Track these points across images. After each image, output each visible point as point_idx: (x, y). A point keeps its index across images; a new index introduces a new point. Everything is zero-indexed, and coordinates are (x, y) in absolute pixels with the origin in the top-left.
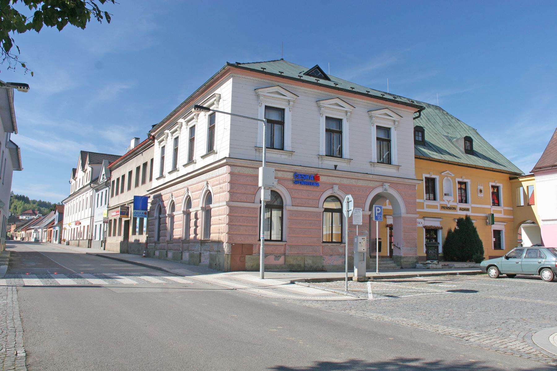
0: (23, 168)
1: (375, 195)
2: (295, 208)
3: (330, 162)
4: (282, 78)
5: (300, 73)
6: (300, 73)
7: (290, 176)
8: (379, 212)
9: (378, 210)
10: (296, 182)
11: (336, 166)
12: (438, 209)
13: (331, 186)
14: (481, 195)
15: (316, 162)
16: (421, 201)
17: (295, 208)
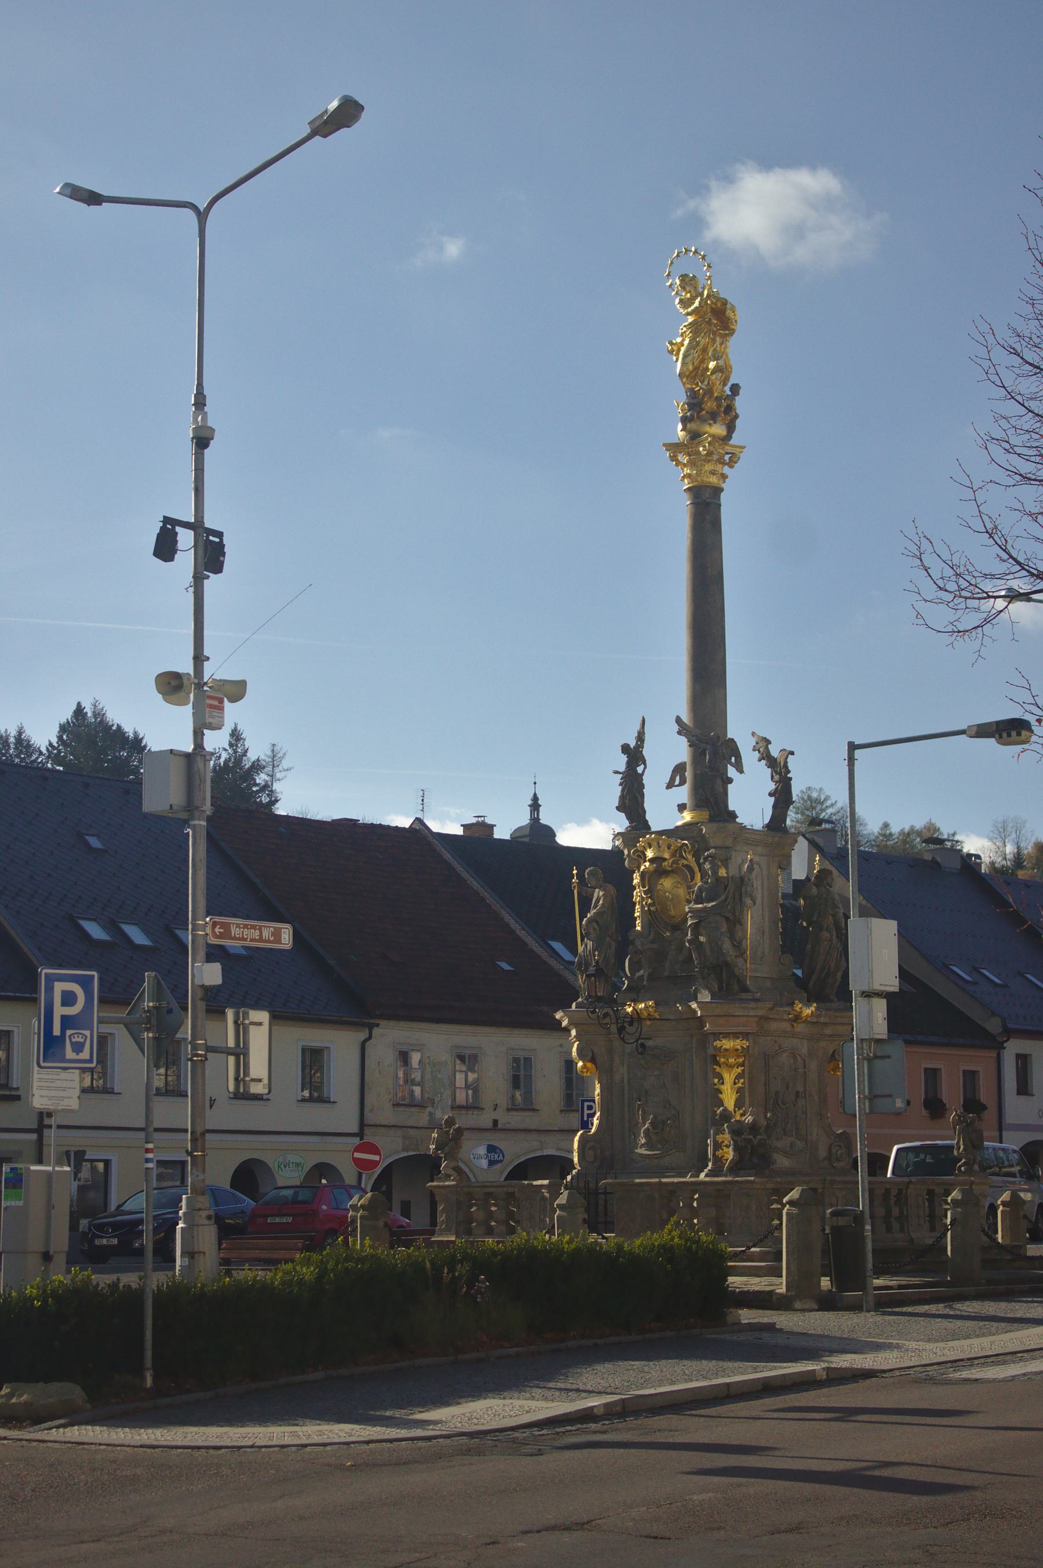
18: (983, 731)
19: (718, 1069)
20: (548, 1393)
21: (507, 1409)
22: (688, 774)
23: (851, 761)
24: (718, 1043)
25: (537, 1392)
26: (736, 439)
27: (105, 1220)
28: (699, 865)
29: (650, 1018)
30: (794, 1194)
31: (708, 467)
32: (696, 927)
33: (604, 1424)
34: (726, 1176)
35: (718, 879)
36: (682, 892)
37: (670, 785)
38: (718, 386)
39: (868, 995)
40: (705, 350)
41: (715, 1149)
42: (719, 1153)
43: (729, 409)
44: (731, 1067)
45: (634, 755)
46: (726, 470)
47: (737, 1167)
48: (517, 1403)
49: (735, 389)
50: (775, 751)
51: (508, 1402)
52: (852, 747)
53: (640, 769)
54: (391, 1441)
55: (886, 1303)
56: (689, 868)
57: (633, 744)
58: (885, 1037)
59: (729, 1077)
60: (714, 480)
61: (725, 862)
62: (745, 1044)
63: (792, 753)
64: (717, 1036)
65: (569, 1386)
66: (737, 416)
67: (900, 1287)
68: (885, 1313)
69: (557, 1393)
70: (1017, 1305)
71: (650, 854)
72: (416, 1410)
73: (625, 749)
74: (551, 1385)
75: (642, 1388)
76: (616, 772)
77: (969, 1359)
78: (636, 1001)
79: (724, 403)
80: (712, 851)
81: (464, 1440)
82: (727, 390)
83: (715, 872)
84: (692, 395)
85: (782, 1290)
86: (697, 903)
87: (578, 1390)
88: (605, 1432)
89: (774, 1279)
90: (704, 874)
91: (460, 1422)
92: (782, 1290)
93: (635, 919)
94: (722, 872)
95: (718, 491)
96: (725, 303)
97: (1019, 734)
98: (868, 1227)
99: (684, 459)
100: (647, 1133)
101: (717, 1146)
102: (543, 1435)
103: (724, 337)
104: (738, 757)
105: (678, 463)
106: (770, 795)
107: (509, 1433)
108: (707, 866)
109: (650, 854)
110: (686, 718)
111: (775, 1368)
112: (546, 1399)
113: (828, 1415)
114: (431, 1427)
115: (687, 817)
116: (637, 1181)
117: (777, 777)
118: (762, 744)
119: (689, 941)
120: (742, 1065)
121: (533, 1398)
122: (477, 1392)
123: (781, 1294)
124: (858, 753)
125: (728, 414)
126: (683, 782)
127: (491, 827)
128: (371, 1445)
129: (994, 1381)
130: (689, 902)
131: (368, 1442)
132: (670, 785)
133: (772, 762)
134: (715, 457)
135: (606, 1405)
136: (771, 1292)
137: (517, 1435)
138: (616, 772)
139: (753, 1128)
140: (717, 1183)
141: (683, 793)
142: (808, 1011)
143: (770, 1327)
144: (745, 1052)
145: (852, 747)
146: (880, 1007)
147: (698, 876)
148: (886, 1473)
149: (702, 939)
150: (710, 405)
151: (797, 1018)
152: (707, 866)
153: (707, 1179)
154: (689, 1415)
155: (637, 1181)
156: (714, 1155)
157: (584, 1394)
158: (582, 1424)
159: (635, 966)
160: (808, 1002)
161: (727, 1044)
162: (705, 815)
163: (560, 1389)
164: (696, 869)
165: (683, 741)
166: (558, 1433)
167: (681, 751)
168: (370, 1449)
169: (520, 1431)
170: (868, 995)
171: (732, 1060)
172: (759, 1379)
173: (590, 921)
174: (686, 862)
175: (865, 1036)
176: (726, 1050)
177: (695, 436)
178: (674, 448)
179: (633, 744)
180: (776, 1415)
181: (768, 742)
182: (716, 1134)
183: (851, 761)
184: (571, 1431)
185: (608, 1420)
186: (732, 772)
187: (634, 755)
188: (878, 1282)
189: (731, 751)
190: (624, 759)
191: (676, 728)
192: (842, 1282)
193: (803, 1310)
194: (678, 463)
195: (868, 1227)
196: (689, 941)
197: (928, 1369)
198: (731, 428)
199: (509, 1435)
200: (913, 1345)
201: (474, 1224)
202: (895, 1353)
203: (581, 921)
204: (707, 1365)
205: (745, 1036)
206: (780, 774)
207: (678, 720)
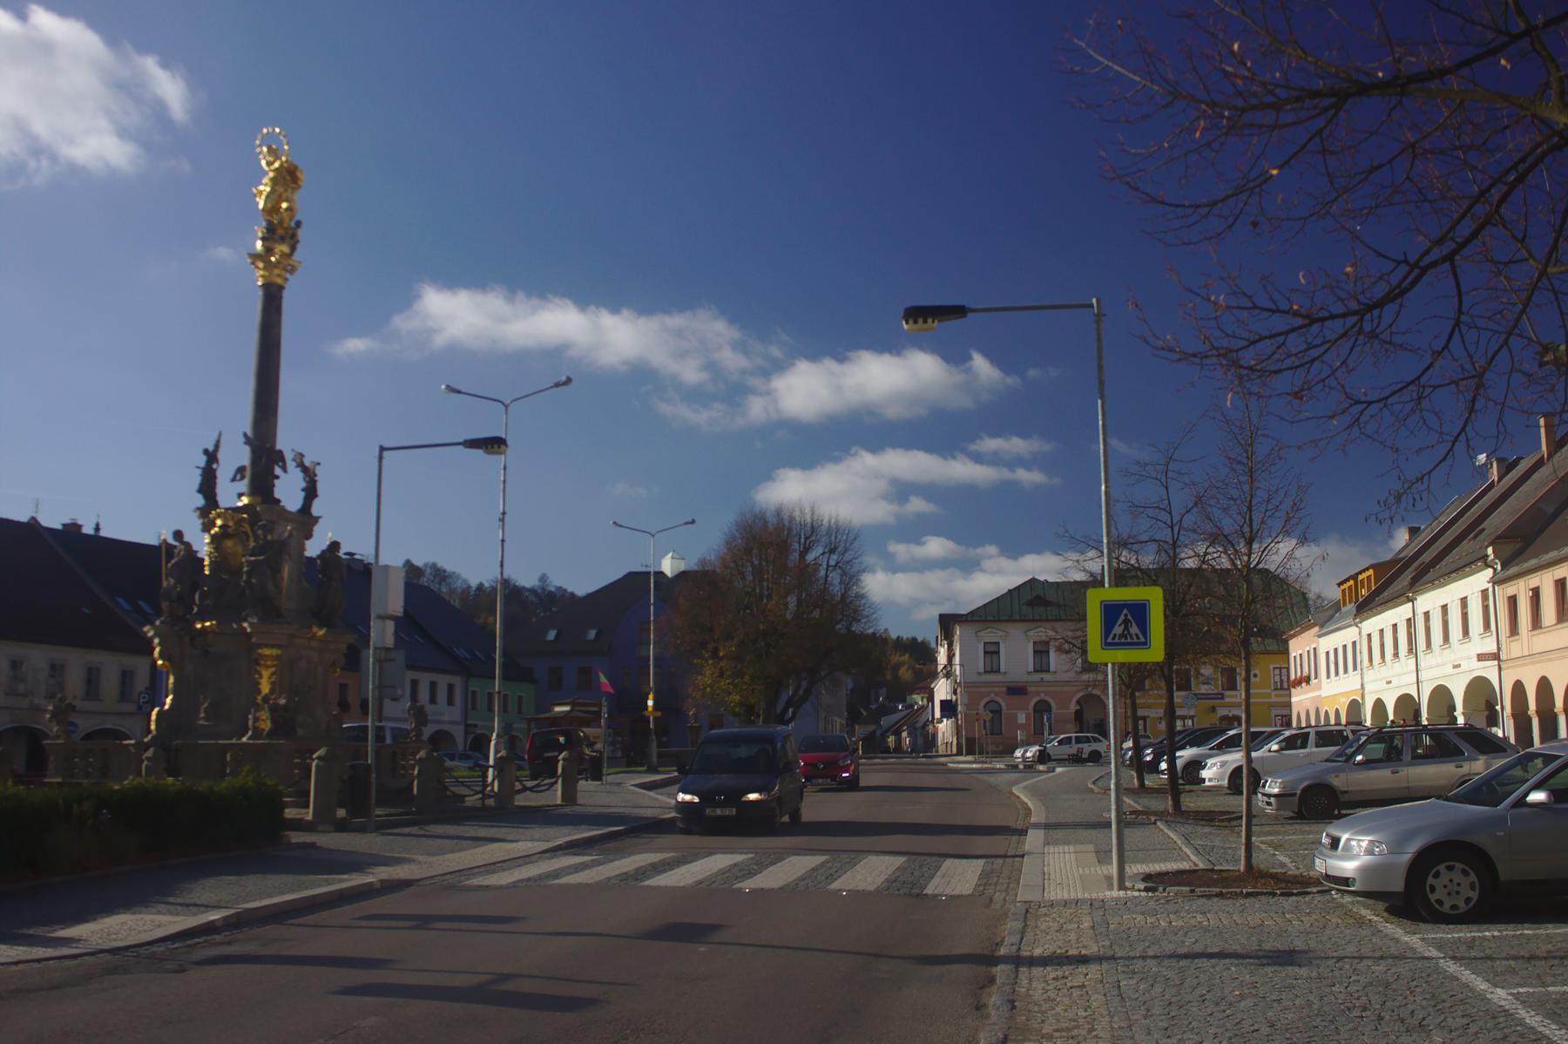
0: (543, 578)
1: (1465, 693)
2: (1059, 711)
3: (1037, 677)
4: (1011, 588)
5: (1400, 479)
6: (1400, 479)
7: (1004, 689)
8: (145, 700)
9: (144, 698)
10: (1008, 694)
11: (1042, 679)
12: (941, 701)
13: (1038, 693)
14: (1258, 679)
15: (1026, 678)
16: (1269, 691)
17: (1059, 711)
18: (473, 444)
19: (258, 668)
20: (172, 908)
21: (139, 923)
22: (248, 473)
23: (381, 458)
24: (260, 651)
25: (162, 907)
26: (297, 256)
27: (961, 766)
28: (252, 530)
29: (213, 632)
30: (321, 752)
31: (276, 271)
32: (249, 573)
33: (226, 935)
34: (264, 739)
35: (266, 542)
36: (240, 549)
37: (234, 480)
38: (287, 220)
39: (382, 617)
40: (280, 195)
41: (254, 722)
42: (257, 724)
43: (294, 236)
44: (267, 667)
45: (212, 456)
46: (288, 276)
47: (272, 734)
48: (149, 917)
49: (298, 224)
50: (307, 463)
51: (139, 916)
52: (382, 449)
53: (214, 466)
54: (39, 961)
55: (382, 827)
56: (246, 533)
57: (211, 448)
58: (392, 646)
59: (266, 674)
60: (279, 281)
61: (271, 531)
62: (279, 652)
63: (319, 464)
64: (260, 646)
65: (188, 901)
66: (298, 241)
67: (387, 815)
68: (383, 834)
69: (179, 908)
70: (467, 828)
71: (219, 522)
72: (56, 927)
73: (206, 452)
74: (171, 900)
75: (247, 902)
76: (198, 467)
77: (468, 869)
78: (204, 621)
79: (290, 232)
80: (264, 522)
81: (108, 957)
82: (293, 224)
83: (265, 537)
84: (270, 223)
85: (310, 817)
86: (251, 556)
87: (195, 905)
88: (229, 943)
89: (303, 811)
90: (256, 538)
91: (100, 938)
92: (310, 817)
93: (204, 566)
94: (269, 537)
95: (281, 288)
96: (296, 168)
97: (499, 447)
98: (374, 776)
99: (261, 265)
100: (206, 711)
101: (256, 719)
102: (177, 948)
103: (294, 190)
104: (283, 460)
105: (257, 267)
106: (303, 490)
107: (147, 947)
108: (260, 532)
109: (219, 522)
110: (250, 433)
111: (341, 881)
112: (171, 913)
113: (409, 923)
114: (74, 945)
115: (245, 500)
116: (201, 742)
117: (307, 479)
118: (298, 456)
119: (244, 582)
120: (274, 666)
121: (159, 913)
122: (109, 909)
123: (308, 821)
124: (386, 454)
125: (291, 238)
126: (243, 478)
127: (80, 526)
128: (21, 967)
129: (500, 887)
130: (244, 556)
131: (16, 963)
132: (234, 480)
133: (305, 469)
134: (281, 266)
135: (225, 918)
136: (302, 819)
137: (155, 949)
138: (198, 467)
139: (285, 708)
140: (258, 744)
141: (243, 486)
142: (321, 633)
143: (313, 845)
144: (278, 657)
145: (382, 449)
146: (390, 626)
147: (252, 539)
148: (510, 986)
149: (254, 581)
150: (280, 232)
151: (314, 637)
152: (260, 532)
153: (251, 742)
154: (293, 925)
155: (201, 742)
156: (253, 726)
157: (202, 909)
158: (207, 935)
159: (203, 596)
160: (321, 627)
161: (267, 652)
162: (258, 499)
163: (182, 905)
164: (251, 534)
165: (247, 449)
166: (189, 946)
167: (243, 456)
168: (19, 970)
169: (157, 945)
170: (382, 617)
171: (269, 663)
172: (334, 891)
173: (174, 565)
174: (244, 529)
175: (379, 645)
176: (266, 656)
177: (269, 251)
178: (255, 257)
179: (211, 448)
180: (364, 923)
181: (302, 456)
182: (255, 712)
183: (381, 458)
184: (199, 943)
185: (229, 931)
186: (278, 471)
187: (212, 456)
188: (379, 812)
189: (279, 458)
190: (204, 458)
191: (243, 439)
192: (353, 813)
193: (324, 832)
194: (257, 267)
195: (374, 776)
196: (244, 582)
197: (447, 877)
198: (293, 248)
199: (147, 950)
200: (421, 858)
201: (76, 770)
202: (413, 866)
203: (167, 564)
204: (289, 879)
205: (278, 646)
206: (310, 477)
207: (245, 435)
